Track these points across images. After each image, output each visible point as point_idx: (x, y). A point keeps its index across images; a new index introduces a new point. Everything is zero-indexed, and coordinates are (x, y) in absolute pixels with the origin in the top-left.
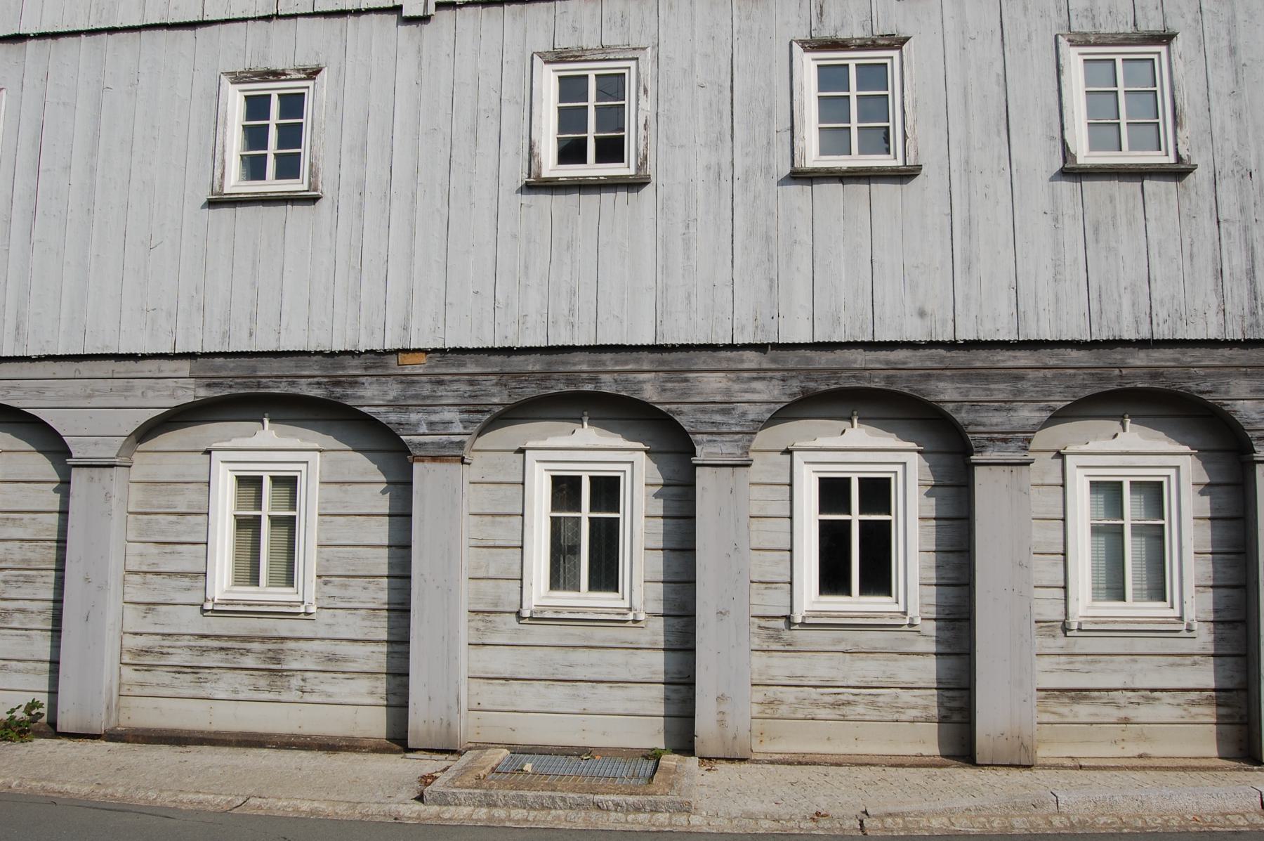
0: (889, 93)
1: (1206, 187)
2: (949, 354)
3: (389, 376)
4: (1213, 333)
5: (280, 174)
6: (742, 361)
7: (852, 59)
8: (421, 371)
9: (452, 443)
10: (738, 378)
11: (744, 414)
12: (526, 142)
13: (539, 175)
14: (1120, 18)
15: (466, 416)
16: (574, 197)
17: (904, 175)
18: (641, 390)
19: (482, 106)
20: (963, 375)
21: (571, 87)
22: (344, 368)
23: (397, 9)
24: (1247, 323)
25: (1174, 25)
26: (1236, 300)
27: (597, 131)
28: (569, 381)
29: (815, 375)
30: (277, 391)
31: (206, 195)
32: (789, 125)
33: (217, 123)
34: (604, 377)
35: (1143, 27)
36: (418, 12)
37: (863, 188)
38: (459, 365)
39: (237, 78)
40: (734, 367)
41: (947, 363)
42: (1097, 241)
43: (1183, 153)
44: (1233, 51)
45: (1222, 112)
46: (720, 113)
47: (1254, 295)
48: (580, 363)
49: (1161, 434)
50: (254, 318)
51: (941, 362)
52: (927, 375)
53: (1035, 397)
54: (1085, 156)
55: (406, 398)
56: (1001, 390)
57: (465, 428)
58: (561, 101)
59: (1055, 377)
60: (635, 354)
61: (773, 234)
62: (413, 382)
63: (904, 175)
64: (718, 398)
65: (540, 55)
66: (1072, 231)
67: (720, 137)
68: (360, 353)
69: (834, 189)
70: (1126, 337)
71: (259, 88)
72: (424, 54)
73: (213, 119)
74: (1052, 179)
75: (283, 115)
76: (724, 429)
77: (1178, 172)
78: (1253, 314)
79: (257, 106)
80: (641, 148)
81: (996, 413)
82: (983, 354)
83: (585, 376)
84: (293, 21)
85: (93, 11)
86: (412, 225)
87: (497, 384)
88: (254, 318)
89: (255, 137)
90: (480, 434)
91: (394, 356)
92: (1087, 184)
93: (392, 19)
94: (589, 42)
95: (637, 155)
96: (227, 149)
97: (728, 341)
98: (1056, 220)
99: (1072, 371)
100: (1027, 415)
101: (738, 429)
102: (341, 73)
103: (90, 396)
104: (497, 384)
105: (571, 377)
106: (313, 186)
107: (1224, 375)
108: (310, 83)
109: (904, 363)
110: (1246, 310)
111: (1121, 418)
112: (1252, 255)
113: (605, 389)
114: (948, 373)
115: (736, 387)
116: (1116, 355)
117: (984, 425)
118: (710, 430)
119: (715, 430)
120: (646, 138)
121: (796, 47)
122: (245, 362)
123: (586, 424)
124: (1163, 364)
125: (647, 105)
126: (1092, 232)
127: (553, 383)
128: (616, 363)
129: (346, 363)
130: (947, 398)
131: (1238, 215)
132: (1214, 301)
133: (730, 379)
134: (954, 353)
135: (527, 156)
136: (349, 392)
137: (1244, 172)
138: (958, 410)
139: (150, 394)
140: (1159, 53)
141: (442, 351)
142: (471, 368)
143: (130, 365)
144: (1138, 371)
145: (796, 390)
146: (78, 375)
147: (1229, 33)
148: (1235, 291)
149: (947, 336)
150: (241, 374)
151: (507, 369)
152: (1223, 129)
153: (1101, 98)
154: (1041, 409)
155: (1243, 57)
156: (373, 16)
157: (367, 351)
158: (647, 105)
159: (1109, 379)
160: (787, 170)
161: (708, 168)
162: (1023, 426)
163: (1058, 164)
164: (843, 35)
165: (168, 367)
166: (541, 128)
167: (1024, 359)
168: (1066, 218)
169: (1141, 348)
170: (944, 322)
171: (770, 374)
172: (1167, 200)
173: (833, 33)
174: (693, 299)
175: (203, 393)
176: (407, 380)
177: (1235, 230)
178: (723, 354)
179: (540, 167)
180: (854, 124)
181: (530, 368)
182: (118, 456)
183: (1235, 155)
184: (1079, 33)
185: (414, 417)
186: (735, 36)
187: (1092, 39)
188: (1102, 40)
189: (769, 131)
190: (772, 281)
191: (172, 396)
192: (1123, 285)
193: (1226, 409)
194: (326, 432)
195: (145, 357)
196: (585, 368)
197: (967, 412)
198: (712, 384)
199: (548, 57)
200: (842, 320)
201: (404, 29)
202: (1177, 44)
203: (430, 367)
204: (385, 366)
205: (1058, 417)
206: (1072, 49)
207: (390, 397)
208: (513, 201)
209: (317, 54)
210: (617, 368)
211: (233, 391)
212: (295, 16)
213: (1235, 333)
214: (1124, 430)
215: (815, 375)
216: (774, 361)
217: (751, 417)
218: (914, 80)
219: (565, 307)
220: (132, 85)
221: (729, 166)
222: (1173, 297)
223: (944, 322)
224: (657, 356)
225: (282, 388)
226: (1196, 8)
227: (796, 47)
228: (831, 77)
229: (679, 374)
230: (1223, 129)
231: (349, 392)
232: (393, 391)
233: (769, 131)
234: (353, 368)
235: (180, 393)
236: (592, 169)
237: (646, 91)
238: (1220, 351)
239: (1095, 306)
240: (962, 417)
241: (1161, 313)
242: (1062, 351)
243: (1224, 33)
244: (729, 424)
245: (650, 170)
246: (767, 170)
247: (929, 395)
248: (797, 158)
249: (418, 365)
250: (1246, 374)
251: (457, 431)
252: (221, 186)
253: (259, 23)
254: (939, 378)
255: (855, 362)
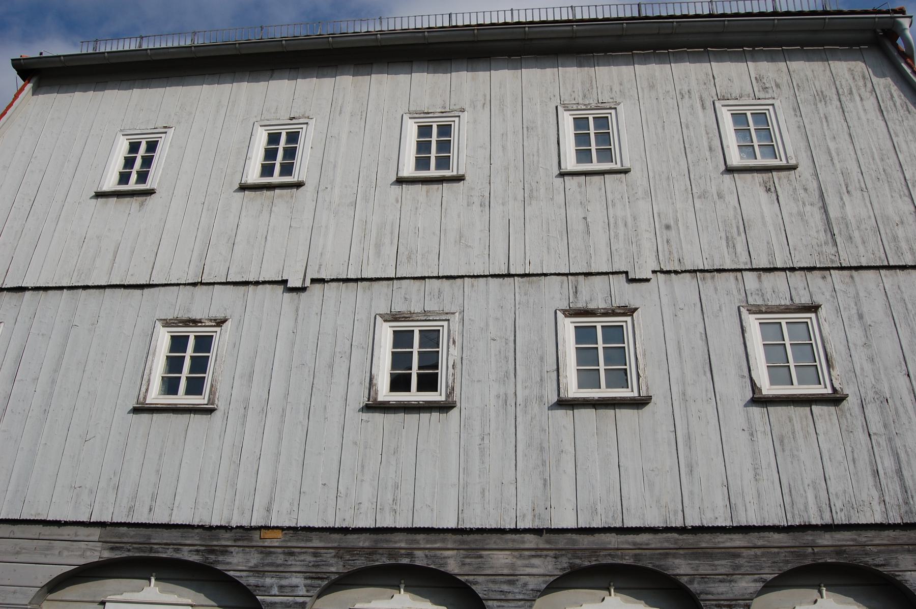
0: (626, 345)
1: (857, 410)
2: (681, 537)
3: (253, 547)
4: (878, 519)
5: (189, 392)
6: (523, 542)
7: (599, 323)
8: (277, 544)
9: (296, 603)
10: (521, 556)
11: (525, 584)
12: (368, 375)
13: (376, 399)
14: (781, 295)
15: (309, 582)
16: (401, 416)
17: (640, 403)
18: (446, 564)
19: (337, 350)
20: (693, 553)
21: (402, 339)
22: (218, 539)
23: (284, 282)
24: (902, 511)
25: (818, 299)
26: (892, 493)
27: (420, 347)
28: (390, 556)
29: (579, 553)
30: (164, 556)
31: (133, 403)
32: (555, 367)
33: (149, 353)
34: (418, 553)
35: (797, 301)
36: (298, 284)
37: (611, 412)
38: (307, 541)
39: (167, 323)
40: (518, 547)
41: (680, 544)
42: (783, 450)
43: (837, 386)
44: (861, 317)
45: (860, 357)
46: (506, 358)
47: (905, 489)
48: (400, 541)
49: (851, 600)
50: (154, 498)
51: (676, 543)
52: (666, 554)
53: (749, 570)
54: (768, 389)
55: (264, 565)
56: (723, 566)
57: (307, 591)
58: (394, 348)
59: (763, 555)
60: (442, 536)
61: (545, 445)
62: (271, 553)
63: (640, 403)
64: (506, 572)
65: (381, 316)
66: (764, 443)
67: (506, 375)
68: (232, 528)
69: (588, 414)
70: (814, 522)
71: (181, 331)
72: (300, 312)
73: (146, 351)
74: (746, 406)
75: (196, 350)
76: (510, 597)
77: (835, 400)
78: (906, 503)
79: (178, 343)
80: (450, 382)
81: (722, 584)
82: (707, 537)
83: (403, 551)
84: (211, 287)
85: (76, 273)
86: (280, 432)
87: (335, 557)
88: (154, 498)
89: (174, 364)
90: (319, 596)
91: (258, 532)
92: (771, 409)
93: (280, 288)
94: (416, 308)
95: (447, 386)
96: (153, 372)
97: (513, 526)
98: (752, 435)
99: (776, 550)
100: (746, 585)
101: (521, 597)
102: (240, 322)
103: (18, 553)
104: (335, 557)
105: (393, 553)
106: (211, 401)
107: (892, 551)
108: (218, 329)
109: (647, 544)
110: (901, 500)
111: (818, 588)
112: (898, 458)
113: (418, 563)
114: (681, 552)
115: (519, 562)
116: (808, 537)
117: (713, 594)
118: (499, 597)
119: (503, 597)
120: (453, 375)
121: (560, 314)
122: (143, 531)
123: (402, 590)
124: (844, 543)
125: (455, 352)
126: (779, 443)
127: (378, 556)
128: (428, 542)
129: (221, 536)
130: (682, 572)
131: (883, 430)
132: (875, 494)
133: (514, 557)
134: (685, 537)
135: (368, 385)
136: (220, 558)
137: (882, 399)
138: (691, 582)
139: (65, 553)
140: (810, 318)
141: (295, 529)
142: (316, 543)
143: (54, 529)
144: (826, 549)
145: (566, 565)
146: (11, 536)
147: (856, 305)
148: (890, 485)
149: (679, 523)
150: (138, 540)
151: (344, 545)
152: (862, 369)
153: (774, 350)
154: (755, 581)
155: (868, 320)
156: (267, 286)
157: (237, 527)
158: (455, 352)
159: (805, 556)
160: (555, 399)
161: (498, 397)
162: (743, 595)
163: (749, 395)
164: (592, 306)
165: (83, 532)
166: (379, 366)
167: (738, 540)
168: (759, 433)
169: (826, 531)
170: (676, 512)
171: (545, 553)
172: (830, 420)
173: (584, 305)
174: (487, 494)
175: (107, 555)
176: (266, 551)
177: (883, 441)
178: (509, 536)
179: (376, 394)
180: (602, 367)
181: (361, 544)
182: (30, 603)
183: (873, 386)
184: (754, 305)
185: (268, 581)
186: (517, 307)
187: (764, 309)
188: (770, 310)
189: (541, 372)
190: (545, 480)
191: (82, 556)
192: (806, 482)
193: (898, 578)
194: (198, 590)
195: (67, 524)
196: (403, 545)
197: (698, 583)
198: (500, 560)
199: (387, 317)
200: (599, 511)
201: (287, 295)
202: (822, 312)
203: (284, 541)
204: (251, 540)
205: (769, 586)
206: (750, 316)
207: (251, 564)
208: (355, 417)
209: (225, 310)
210: (428, 546)
211: (131, 554)
212: (213, 284)
213: (895, 519)
214: (822, 597)
215: (579, 553)
216: (548, 542)
217: (531, 587)
218: (643, 337)
219: (390, 497)
220: (93, 324)
221: (513, 396)
222: (845, 492)
223: (676, 512)
224: (459, 537)
225: (169, 554)
226: (831, 289)
227: (560, 314)
228: (584, 334)
229: (475, 552)
230: (862, 369)
231: (220, 558)
232: (255, 559)
233: (541, 372)
234: (225, 540)
235: (88, 553)
236: (414, 396)
237: (454, 342)
238: (886, 533)
239: (787, 499)
240: (695, 587)
241: (838, 504)
242: (766, 534)
243: (853, 305)
244: (514, 593)
245: (456, 398)
246: (541, 398)
247: (668, 569)
248: (562, 390)
249: (275, 540)
250: (909, 551)
251: (301, 593)
252: (145, 398)
253: (188, 287)
254: (675, 556)
255: (610, 543)
